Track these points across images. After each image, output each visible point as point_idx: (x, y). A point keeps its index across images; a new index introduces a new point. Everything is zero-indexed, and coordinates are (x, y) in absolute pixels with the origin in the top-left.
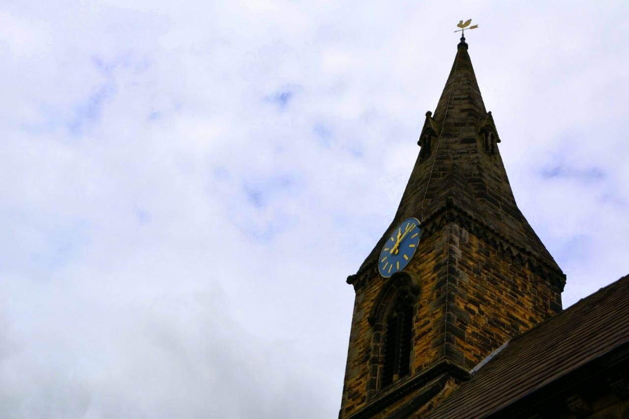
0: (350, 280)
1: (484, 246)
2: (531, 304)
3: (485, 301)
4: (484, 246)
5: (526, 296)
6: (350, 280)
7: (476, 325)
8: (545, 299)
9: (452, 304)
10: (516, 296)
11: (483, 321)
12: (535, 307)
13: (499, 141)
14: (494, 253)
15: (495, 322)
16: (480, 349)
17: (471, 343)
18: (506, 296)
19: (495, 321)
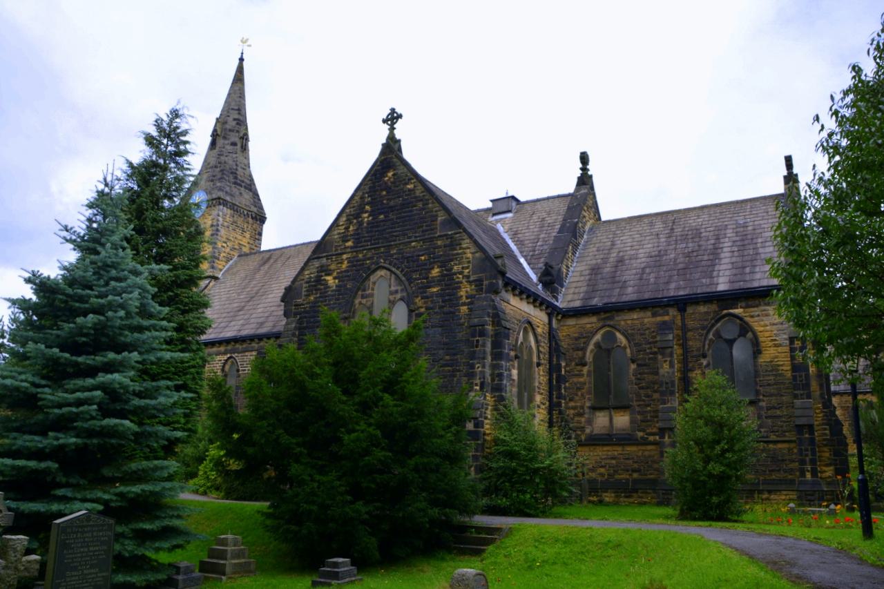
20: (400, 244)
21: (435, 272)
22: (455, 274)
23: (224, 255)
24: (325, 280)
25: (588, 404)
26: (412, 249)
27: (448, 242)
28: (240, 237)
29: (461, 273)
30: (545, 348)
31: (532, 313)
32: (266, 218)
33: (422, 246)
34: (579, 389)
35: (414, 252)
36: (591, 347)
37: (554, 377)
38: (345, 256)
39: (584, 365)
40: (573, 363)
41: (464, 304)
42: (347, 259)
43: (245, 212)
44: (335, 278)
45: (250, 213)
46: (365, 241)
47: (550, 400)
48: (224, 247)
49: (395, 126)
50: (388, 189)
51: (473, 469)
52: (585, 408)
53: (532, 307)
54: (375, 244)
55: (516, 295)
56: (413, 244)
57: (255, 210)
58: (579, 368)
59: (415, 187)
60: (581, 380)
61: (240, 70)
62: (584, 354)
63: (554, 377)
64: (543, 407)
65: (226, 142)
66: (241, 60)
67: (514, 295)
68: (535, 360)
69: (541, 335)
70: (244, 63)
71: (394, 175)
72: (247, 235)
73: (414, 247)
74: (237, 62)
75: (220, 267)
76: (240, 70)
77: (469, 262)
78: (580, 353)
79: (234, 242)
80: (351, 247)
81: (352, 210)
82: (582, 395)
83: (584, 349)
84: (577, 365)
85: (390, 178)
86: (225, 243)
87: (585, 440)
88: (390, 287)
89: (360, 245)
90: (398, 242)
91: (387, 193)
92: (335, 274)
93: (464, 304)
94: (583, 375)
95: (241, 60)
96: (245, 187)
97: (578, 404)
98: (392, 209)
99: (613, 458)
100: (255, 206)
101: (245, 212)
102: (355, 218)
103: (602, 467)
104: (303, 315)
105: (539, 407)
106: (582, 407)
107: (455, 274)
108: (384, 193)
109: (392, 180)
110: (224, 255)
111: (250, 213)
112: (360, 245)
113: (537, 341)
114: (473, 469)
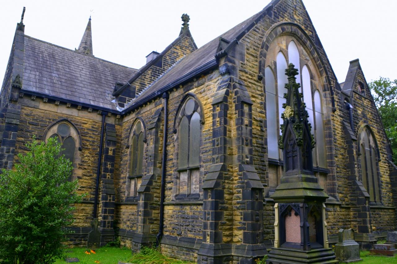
105: (79, 178)
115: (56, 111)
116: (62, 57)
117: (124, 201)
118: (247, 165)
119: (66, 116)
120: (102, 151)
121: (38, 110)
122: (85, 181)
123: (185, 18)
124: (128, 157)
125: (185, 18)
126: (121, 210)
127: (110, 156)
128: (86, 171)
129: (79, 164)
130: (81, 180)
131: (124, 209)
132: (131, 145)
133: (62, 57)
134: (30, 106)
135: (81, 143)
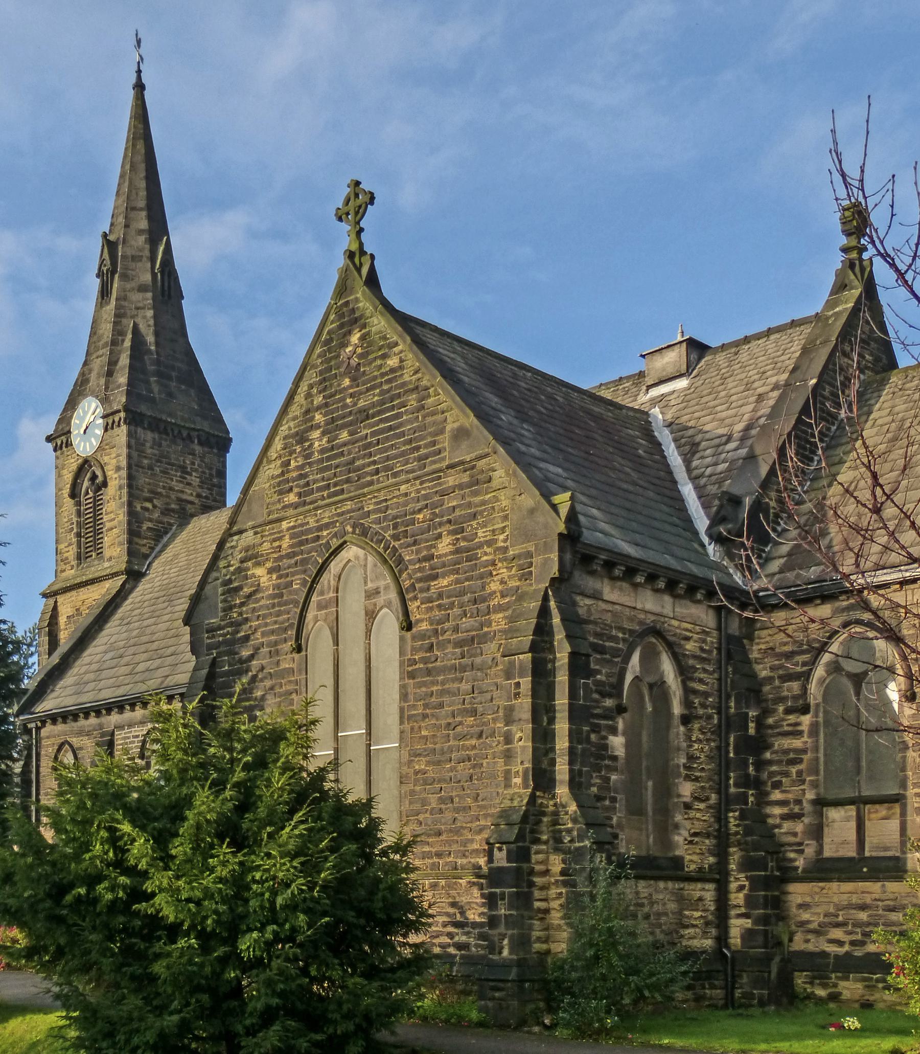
0: (49, 439)
1: (19, 936)
2: (198, 480)
3: (160, 494)
4: (19, 936)
5: (194, 474)
6: (49, 439)
7: (150, 520)
8: (210, 469)
9: (13, 910)
10: (185, 478)
11: (156, 515)
12: (201, 482)
13: (560, 535)
14: (166, 440)
15: (166, 512)
16: (154, 539)
17: (146, 538)
18: (177, 481)
19: (167, 510)
20: (379, 490)
21: (444, 546)
22: (480, 546)
23: (150, 525)
24: (253, 575)
25: (810, 795)
26: (402, 500)
27: (465, 478)
28: (179, 487)
29: (489, 543)
30: (706, 680)
31: (668, 611)
32: (230, 440)
33: (418, 491)
34: (793, 762)
35: (406, 504)
36: (820, 672)
37: (732, 739)
38: (285, 525)
39: (805, 710)
40: (781, 709)
41: (500, 608)
42: (289, 529)
43: (185, 433)
44: (270, 571)
45: (195, 434)
46: (320, 489)
47: (721, 788)
48: (147, 509)
49: (362, 224)
50: (355, 374)
51: (506, 942)
52: (805, 804)
53: (667, 599)
54: (336, 494)
55: (617, 579)
56: (403, 487)
57: (206, 426)
58: (792, 718)
59: (401, 361)
60: (797, 743)
61: (141, 114)
62: (804, 689)
63: (732, 739)
64: (702, 806)
65: (128, 286)
66: (140, 87)
67: (613, 579)
68: (677, 709)
69: (695, 657)
70: (147, 93)
71: (363, 338)
72: (195, 479)
73: (406, 494)
74: (130, 95)
75: (145, 550)
76: (141, 114)
77: (506, 518)
78: (795, 686)
79: (168, 497)
80: (295, 506)
81: (292, 424)
82: (799, 773)
83: (805, 677)
84: (788, 711)
85: (356, 346)
86: (149, 500)
87: (804, 871)
88: (366, 583)
89: (308, 499)
90: (376, 487)
91: (353, 379)
92: (269, 565)
93: (500, 608)
94: (800, 733)
95: (140, 87)
96: (180, 380)
97: (790, 796)
98: (365, 415)
99: (863, 907)
100: (205, 417)
101: (185, 433)
102: (298, 443)
103: (838, 925)
104: (222, 649)
105: (688, 806)
106: (798, 802)
107: (480, 546)
108: (347, 382)
109: (359, 350)
110: (150, 525)
111: (195, 434)
112: (308, 499)
113: (684, 672)
114: (506, 942)
115: (634, 605)
116: (755, 371)
117: (800, 870)
118: (398, 731)
119: (653, 618)
120: (729, 724)
121: (600, 603)
122: (698, 815)
123: (916, 163)
124: (805, 739)
125: (916, 163)
126: (790, 898)
127: (751, 736)
128: (698, 784)
129: (685, 766)
130: (692, 814)
131: (797, 892)
132: (817, 705)
133: (755, 371)
134: (887, 565)
135: (687, 703)
